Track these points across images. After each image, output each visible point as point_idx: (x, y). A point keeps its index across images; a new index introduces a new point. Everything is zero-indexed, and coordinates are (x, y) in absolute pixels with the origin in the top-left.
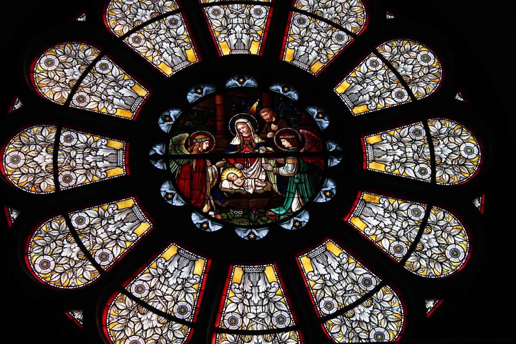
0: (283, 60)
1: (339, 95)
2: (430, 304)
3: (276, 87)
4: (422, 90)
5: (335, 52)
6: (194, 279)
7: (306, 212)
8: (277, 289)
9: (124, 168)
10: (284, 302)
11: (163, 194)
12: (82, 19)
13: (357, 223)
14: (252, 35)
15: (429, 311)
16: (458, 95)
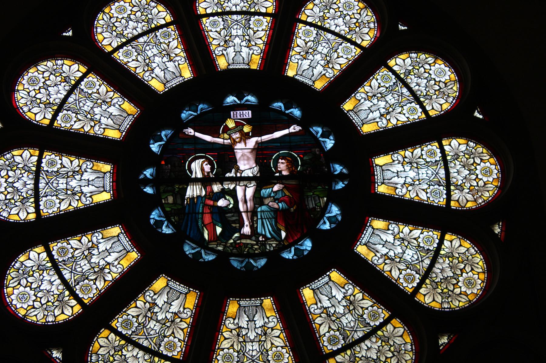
0: (286, 74)
1: (346, 112)
2: (444, 340)
3: (276, 104)
4: (437, 106)
5: (342, 66)
6: (185, 313)
7: (308, 240)
8: (275, 324)
9: (112, 193)
10: (210, 37)
11: (152, 222)
12: (67, 34)
13: (128, 106)
14: (252, 47)
15: (441, 348)
16: (476, 111)
